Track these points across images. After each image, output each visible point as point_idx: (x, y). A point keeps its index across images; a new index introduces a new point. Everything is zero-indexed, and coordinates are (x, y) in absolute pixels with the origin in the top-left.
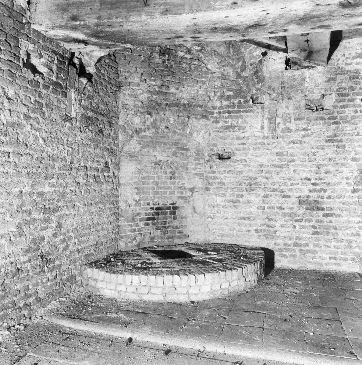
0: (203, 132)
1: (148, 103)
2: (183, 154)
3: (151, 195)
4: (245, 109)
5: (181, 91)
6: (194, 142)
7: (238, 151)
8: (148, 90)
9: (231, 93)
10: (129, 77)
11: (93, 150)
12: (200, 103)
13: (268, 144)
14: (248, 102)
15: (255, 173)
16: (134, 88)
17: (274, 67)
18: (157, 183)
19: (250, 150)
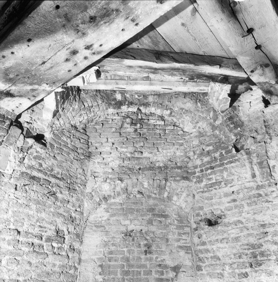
0: (184, 194)
1: (119, 169)
2: (161, 222)
3: (119, 276)
4: (228, 160)
5: (156, 154)
6: (175, 207)
7: (229, 210)
8: (119, 157)
9: (211, 148)
10: (100, 147)
11: (36, 213)
12: (179, 164)
13: (266, 195)
14: (230, 152)
15: (258, 237)
16: (104, 156)
17: (252, 109)
18: (128, 260)
19: (244, 208)
